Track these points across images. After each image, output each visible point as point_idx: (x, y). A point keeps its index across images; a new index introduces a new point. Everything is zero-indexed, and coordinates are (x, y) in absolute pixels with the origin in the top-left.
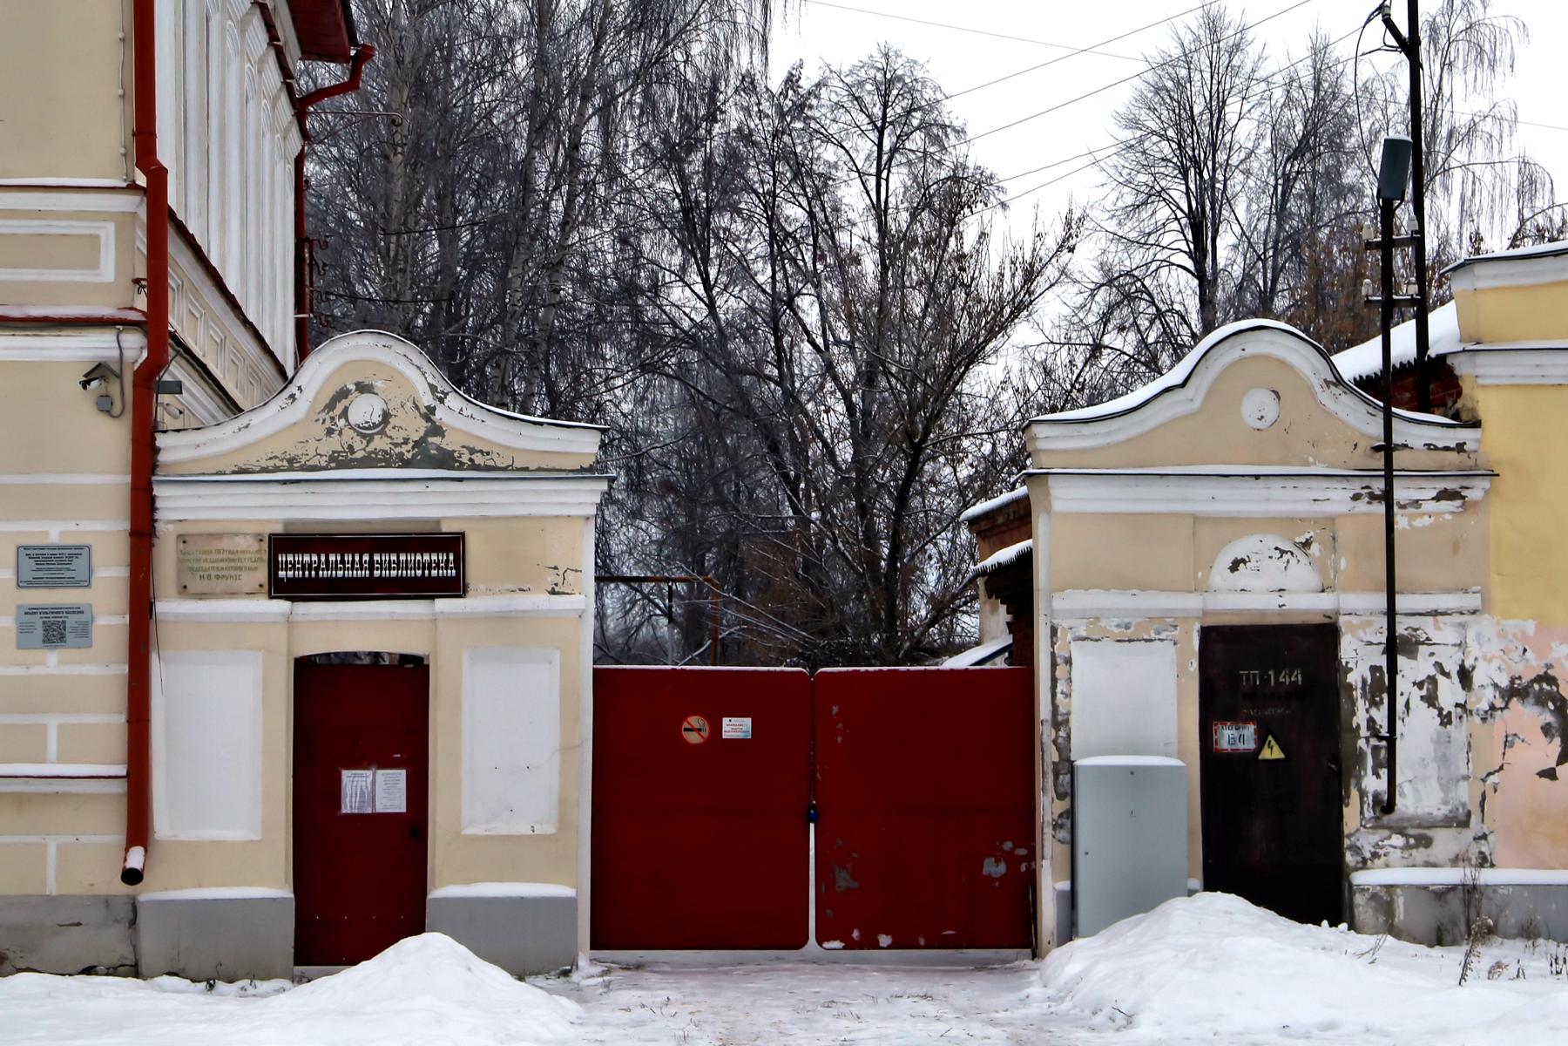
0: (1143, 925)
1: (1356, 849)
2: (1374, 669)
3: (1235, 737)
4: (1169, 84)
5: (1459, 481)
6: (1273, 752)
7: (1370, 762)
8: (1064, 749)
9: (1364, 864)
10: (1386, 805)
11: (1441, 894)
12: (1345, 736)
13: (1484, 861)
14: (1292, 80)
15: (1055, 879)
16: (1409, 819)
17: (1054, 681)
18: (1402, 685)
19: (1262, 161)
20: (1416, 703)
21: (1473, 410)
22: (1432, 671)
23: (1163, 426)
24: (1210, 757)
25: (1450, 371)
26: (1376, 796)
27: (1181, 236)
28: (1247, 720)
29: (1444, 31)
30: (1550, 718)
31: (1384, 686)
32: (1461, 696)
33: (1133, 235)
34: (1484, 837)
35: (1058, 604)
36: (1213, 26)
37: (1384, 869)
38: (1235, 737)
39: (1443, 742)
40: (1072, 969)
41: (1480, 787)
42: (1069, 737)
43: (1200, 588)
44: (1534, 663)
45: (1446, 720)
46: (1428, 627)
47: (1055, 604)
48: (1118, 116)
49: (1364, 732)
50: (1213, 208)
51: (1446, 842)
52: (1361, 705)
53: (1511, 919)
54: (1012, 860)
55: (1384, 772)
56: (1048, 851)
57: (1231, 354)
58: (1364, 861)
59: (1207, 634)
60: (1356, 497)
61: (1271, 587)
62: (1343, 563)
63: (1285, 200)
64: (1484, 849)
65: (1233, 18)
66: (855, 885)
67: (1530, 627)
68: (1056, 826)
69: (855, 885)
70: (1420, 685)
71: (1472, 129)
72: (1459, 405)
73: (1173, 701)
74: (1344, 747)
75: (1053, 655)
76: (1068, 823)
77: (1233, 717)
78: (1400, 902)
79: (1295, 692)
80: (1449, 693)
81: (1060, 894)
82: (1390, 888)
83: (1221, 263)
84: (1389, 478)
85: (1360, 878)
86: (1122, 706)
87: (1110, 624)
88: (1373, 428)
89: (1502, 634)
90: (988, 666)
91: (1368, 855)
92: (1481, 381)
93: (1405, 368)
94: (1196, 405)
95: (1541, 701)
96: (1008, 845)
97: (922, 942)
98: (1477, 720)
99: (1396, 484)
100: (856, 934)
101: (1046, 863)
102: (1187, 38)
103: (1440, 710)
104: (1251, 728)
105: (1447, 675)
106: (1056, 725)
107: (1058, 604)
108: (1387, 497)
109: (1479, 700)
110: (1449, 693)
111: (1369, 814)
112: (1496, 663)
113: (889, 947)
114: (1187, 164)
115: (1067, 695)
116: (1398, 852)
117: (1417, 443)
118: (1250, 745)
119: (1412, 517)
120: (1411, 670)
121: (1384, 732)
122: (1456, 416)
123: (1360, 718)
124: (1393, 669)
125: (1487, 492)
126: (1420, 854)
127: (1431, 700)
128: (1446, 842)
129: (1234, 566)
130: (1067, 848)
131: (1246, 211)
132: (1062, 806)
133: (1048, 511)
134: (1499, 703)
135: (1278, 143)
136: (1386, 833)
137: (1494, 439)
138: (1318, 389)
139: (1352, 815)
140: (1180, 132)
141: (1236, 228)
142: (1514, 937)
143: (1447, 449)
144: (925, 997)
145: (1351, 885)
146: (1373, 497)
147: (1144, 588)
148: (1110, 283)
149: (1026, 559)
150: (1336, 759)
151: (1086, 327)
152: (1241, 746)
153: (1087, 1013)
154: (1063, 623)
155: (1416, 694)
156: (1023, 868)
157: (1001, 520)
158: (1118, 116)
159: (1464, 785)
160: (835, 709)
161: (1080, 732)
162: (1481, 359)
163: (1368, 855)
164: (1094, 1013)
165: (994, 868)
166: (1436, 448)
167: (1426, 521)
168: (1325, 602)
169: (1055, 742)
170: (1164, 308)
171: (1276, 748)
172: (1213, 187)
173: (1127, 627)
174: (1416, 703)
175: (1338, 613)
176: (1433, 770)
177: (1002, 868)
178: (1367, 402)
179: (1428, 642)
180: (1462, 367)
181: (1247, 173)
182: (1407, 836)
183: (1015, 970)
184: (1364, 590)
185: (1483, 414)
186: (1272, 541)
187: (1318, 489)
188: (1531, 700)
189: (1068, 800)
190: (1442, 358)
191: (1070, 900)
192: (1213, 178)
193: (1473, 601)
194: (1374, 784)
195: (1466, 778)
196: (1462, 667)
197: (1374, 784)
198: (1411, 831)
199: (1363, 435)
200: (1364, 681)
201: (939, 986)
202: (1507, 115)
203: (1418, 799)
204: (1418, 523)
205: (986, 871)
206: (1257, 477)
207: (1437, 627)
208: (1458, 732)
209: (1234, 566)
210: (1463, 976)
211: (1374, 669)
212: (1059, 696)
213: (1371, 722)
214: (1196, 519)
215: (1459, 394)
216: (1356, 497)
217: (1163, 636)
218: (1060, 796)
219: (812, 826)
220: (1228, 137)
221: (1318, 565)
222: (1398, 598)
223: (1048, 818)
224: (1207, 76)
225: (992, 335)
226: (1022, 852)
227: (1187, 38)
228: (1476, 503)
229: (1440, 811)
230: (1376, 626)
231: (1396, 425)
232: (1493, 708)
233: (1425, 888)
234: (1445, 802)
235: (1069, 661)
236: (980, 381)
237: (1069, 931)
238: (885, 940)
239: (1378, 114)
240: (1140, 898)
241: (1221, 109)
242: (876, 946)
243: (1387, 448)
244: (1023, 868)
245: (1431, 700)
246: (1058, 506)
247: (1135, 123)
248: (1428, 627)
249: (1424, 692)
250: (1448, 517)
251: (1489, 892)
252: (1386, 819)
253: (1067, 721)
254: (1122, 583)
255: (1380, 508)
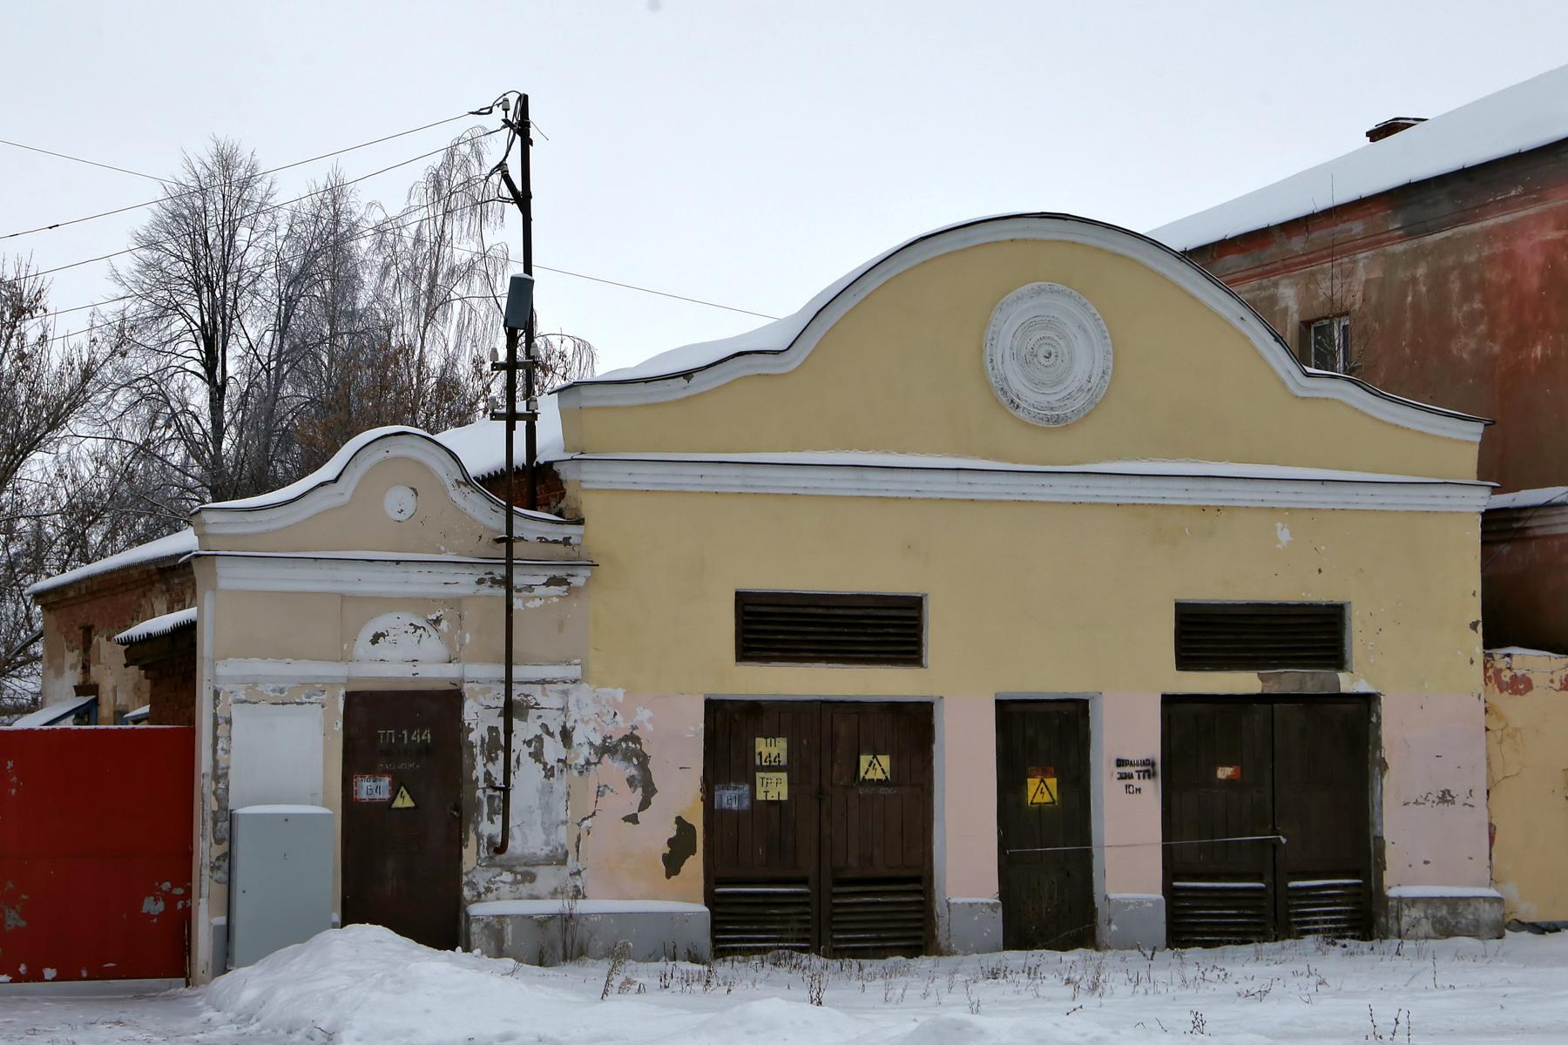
0: (304, 955)
1: (472, 885)
2: (491, 729)
3: (373, 789)
4: (186, 212)
5: (568, 566)
6: (404, 801)
7: (486, 809)
8: (222, 799)
9: (479, 898)
10: (499, 848)
11: (543, 922)
12: (466, 787)
13: (578, 894)
14: (293, 217)
15: (211, 914)
16: (517, 859)
17: (216, 739)
18: (516, 743)
19: (269, 286)
20: (525, 758)
21: (577, 509)
22: (539, 732)
23: (317, 515)
24: (353, 811)
25: (556, 475)
26: (490, 838)
27: (194, 346)
28: (384, 773)
29: (445, 183)
30: (634, 772)
31: (499, 744)
32: (562, 753)
33: (150, 343)
34: (579, 873)
35: (222, 670)
36: (225, 162)
37: (494, 901)
38: (373, 789)
39: (547, 791)
40: (249, 995)
41: (576, 831)
42: (227, 788)
43: (346, 658)
44: (622, 725)
45: (549, 773)
46: (536, 692)
47: (218, 670)
48: (138, 237)
49: (482, 784)
50: (223, 319)
51: (547, 878)
52: (480, 761)
53: (599, 944)
54: (170, 899)
55: (498, 819)
56: (205, 890)
57: (377, 454)
58: (479, 895)
59: (350, 698)
60: (480, 582)
61: (406, 658)
62: (468, 638)
63: (287, 318)
64: (579, 883)
65: (244, 155)
66: (23, 924)
67: (620, 694)
68: (213, 868)
69: (23, 924)
70: (529, 743)
71: (471, 266)
72: (562, 505)
73: (320, 756)
74: (465, 797)
75: (215, 716)
76: (226, 865)
77: (371, 771)
78: (509, 929)
79: (425, 749)
80: (553, 750)
81: (217, 928)
82: (500, 918)
83: (230, 372)
84: (509, 566)
85: (475, 910)
86: (274, 761)
87: (267, 689)
88: (497, 522)
89: (597, 700)
90: (57, 727)
91: (482, 890)
92: (584, 486)
93: (519, 472)
94: (347, 497)
95: (627, 758)
96: (166, 886)
97: (84, 974)
98: (575, 773)
99: (515, 570)
100: (23, 968)
101: (203, 901)
102: (203, 173)
103: (545, 764)
104: (387, 780)
105: (551, 735)
106: (217, 778)
107: (222, 670)
108: (507, 582)
109: (577, 756)
110: (553, 750)
111: (484, 854)
112: (592, 725)
113: (54, 980)
114: (202, 283)
115: (227, 752)
116: (507, 887)
117: (532, 537)
118: (385, 795)
119: (527, 599)
120: (524, 730)
121: (499, 782)
122: (559, 514)
123: (479, 772)
124: (509, 731)
125: (588, 579)
126: (525, 889)
127: (537, 756)
128: (547, 878)
129: (375, 639)
130: (225, 887)
131: (254, 330)
132: (220, 850)
133: (215, 589)
134: (593, 759)
135: (282, 265)
136: (498, 870)
137: (595, 535)
138: (450, 488)
139: (469, 856)
140: (195, 254)
141: (244, 342)
142: (601, 958)
143: (555, 542)
144: (119, 1023)
145: (468, 916)
146: (494, 581)
147: (297, 658)
148: (128, 385)
149: (187, 632)
150: (458, 808)
151: (106, 423)
152: (377, 796)
153: (281, 1032)
154: (225, 688)
155: (526, 750)
156: (180, 906)
157: (71, 594)
158: (138, 237)
159: (563, 829)
160: (10, 764)
161: (237, 785)
162: (585, 467)
163: (482, 890)
164: (290, 1032)
165: (153, 906)
166: (547, 541)
167: (537, 603)
168: (451, 671)
169: (214, 793)
170: (178, 408)
171: (407, 797)
172: (224, 305)
173: (282, 691)
174: (525, 758)
175: (462, 680)
176: (537, 816)
177: (160, 907)
178: (491, 500)
179: (537, 706)
180: (566, 473)
181: (255, 293)
182: (516, 873)
183: (175, 998)
184: (485, 661)
185: (586, 512)
186: (408, 618)
187: (450, 574)
188: (619, 756)
189: (226, 844)
190: (549, 464)
191: (226, 934)
192: (224, 296)
193: (574, 672)
194: (490, 828)
195: (565, 822)
196: (564, 727)
197: (490, 828)
198: (518, 869)
199: (486, 528)
200: (483, 740)
201: (130, 1012)
202: (501, 255)
203: (527, 840)
204: (530, 605)
205: (145, 910)
206: (398, 562)
207: (544, 694)
208: (559, 784)
209: (375, 639)
210: (605, 992)
211: (491, 729)
212: (220, 752)
213: (488, 774)
214: (344, 597)
215: (563, 495)
216: (480, 582)
217: (313, 699)
218: (218, 841)
219: (1292, 884)
220: (238, 262)
221: (447, 640)
222: (514, 668)
223: (206, 861)
224: (220, 207)
225: (53, 426)
226: (179, 891)
227: (203, 173)
228: (578, 589)
229: (543, 851)
230: (494, 692)
231: (516, 520)
232: (588, 762)
233: (530, 917)
234: (547, 843)
235: (229, 722)
236: (36, 468)
237: (225, 962)
238: (49, 973)
239: (389, 250)
240: (299, 931)
241: (232, 237)
242: (41, 979)
243: (509, 540)
244: (180, 906)
245: (537, 756)
246: (223, 584)
247: (152, 244)
248: (536, 692)
249: (532, 750)
250: (555, 600)
251: (582, 920)
252: (498, 858)
253: (226, 774)
254: (280, 654)
255: (502, 592)
